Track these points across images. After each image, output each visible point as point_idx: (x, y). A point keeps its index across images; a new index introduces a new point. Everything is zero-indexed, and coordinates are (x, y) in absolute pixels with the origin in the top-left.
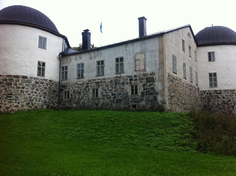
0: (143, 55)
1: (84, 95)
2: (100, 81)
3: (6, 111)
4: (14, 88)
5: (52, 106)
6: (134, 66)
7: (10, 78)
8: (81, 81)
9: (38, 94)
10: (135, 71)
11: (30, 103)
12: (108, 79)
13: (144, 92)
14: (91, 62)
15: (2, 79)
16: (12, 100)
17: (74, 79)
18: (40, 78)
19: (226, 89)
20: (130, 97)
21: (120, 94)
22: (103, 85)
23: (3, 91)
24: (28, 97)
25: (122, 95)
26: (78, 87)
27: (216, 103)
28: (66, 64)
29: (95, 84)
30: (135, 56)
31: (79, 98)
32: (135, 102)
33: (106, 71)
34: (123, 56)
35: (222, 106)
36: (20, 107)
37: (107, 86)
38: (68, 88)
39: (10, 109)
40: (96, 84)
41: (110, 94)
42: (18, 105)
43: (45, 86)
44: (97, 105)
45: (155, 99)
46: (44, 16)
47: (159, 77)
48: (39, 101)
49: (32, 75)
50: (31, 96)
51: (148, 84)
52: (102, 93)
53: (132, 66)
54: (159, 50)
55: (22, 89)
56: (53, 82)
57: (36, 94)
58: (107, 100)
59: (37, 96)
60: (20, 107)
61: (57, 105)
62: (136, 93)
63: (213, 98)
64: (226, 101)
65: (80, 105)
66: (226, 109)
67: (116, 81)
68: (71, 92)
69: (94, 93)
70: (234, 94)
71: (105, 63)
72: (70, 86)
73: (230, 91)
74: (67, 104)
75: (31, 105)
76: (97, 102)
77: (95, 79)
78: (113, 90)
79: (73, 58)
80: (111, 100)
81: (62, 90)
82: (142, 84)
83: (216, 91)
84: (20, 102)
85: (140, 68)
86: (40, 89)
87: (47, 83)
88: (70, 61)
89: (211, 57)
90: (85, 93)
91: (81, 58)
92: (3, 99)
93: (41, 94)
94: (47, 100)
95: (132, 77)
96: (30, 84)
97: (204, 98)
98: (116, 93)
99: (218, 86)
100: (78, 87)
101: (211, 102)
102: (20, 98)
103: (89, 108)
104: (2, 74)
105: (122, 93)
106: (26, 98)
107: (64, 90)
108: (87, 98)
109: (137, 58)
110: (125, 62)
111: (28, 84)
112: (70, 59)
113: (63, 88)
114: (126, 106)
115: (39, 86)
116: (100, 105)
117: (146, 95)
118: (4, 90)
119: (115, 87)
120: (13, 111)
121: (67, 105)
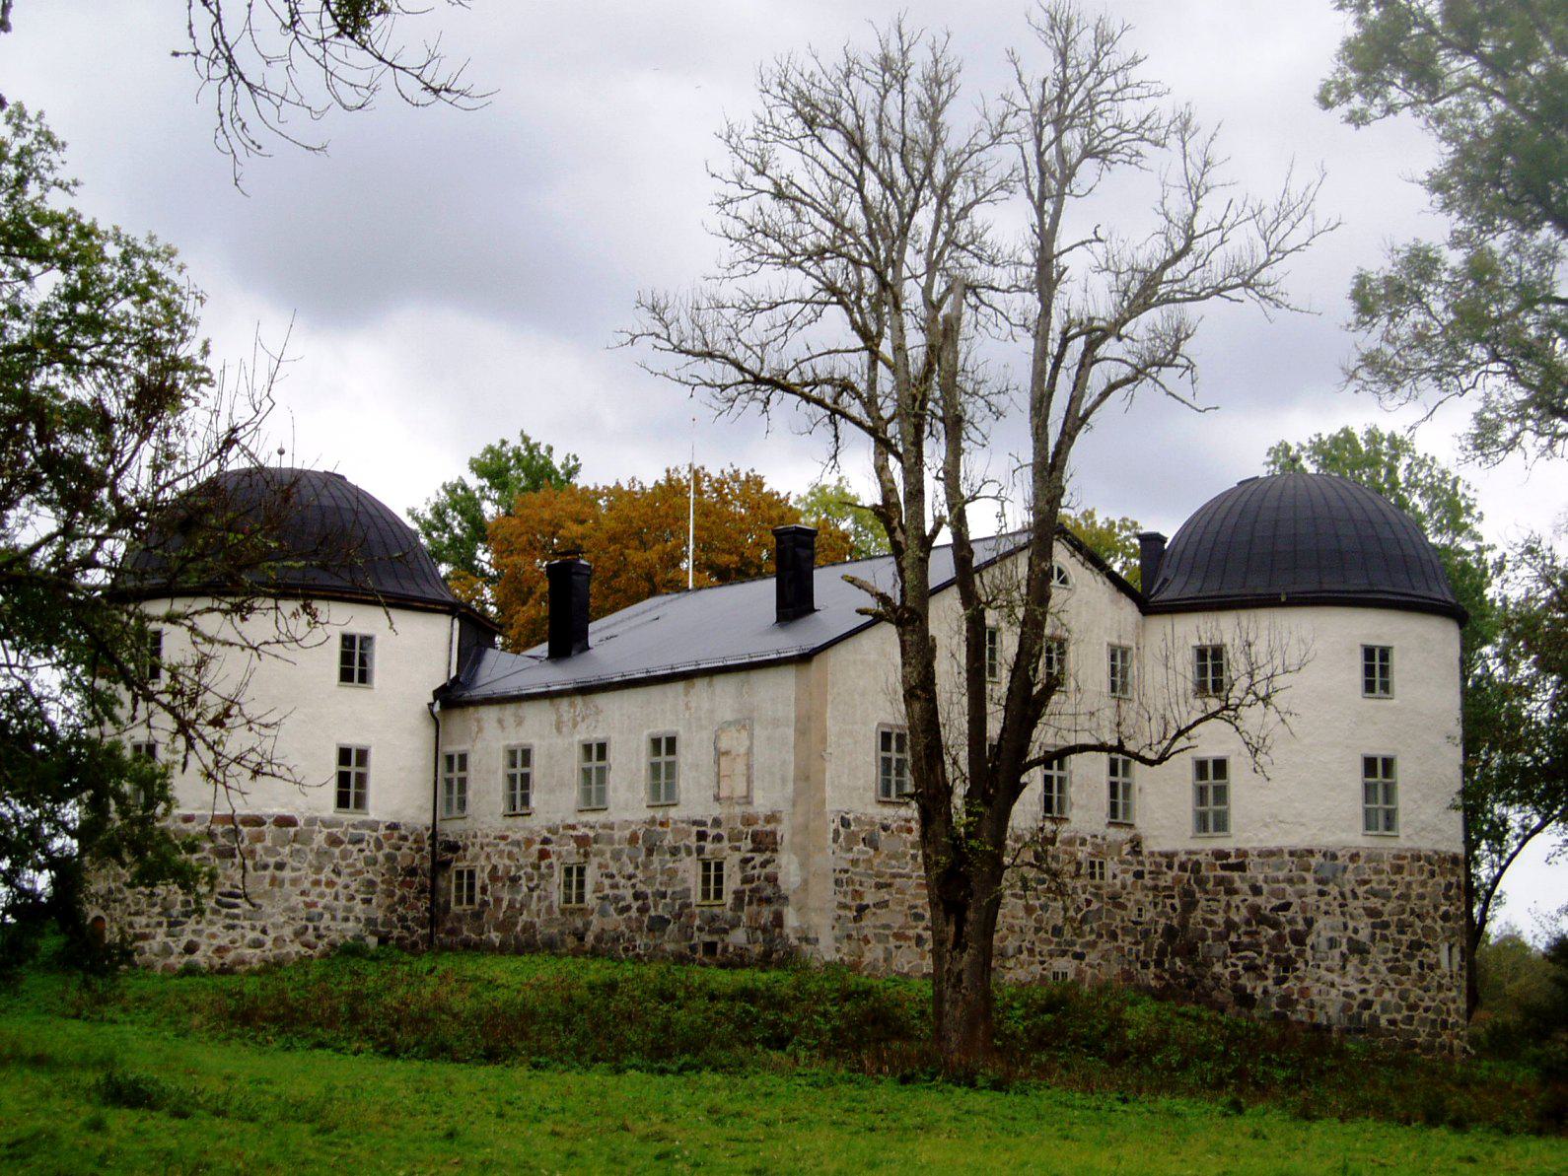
0: (744, 734)
1: (531, 890)
2: (592, 834)
6: (712, 775)
8: (520, 829)
9: (339, 888)
10: (717, 798)
11: (311, 930)
13: (744, 891)
14: (560, 742)
17: (492, 814)
18: (350, 817)
19: (1272, 844)
21: (664, 895)
22: (601, 853)
24: (301, 905)
25: (668, 900)
27: (1219, 919)
29: (573, 845)
30: (717, 738)
31: (511, 905)
32: (711, 932)
33: (615, 790)
34: (675, 729)
35: (1246, 933)
36: (269, 944)
37: (616, 856)
38: (468, 857)
40: (579, 847)
41: (628, 893)
43: (367, 853)
44: (581, 938)
45: (778, 920)
46: (365, 502)
47: (793, 835)
48: (346, 919)
49: (316, 810)
51: (759, 858)
52: (598, 888)
53: (707, 779)
54: (798, 720)
55: (277, 873)
56: (403, 832)
58: (615, 921)
59: (336, 898)
60: (269, 944)
61: (424, 932)
62: (719, 894)
64: (1269, 907)
65: (516, 938)
66: (1266, 949)
67: (648, 842)
68: (482, 877)
69: (568, 885)
70: (1307, 870)
71: (612, 754)
72: (477, 848)
73: (1292, 854)
74: (465, 928)
76: (579, 923)
77: (571, 821)
78: (640, 875)
79: (489, 714)
80: (630, 918)
81: (447, 864)
82: (737, 856)
83: (1221, 855)
85: (733, 790)
86: (348, 866)
90: (535, 882)
91: (520, 723)
93: (354, 886)
94: (380, 915)
95: (704, 824)
96: (307, 849)
97: (1166, 888)
98: (649, 891)
100: (510, 855)
101: (1198, 915)
103: (551, 946)
104: (197, 813)
105: (669, 892)
106: (293, 909)
107: (453, 864)
109: (724, 745)
110: (684, 757)
111: (298, 851)
112: (478, 721)
113: (450, 856)
115: (345, 856)
116: (590, 938)
117: (750, 903)
119: (646, 867)
120: (243, 962)
121: (466, 933)
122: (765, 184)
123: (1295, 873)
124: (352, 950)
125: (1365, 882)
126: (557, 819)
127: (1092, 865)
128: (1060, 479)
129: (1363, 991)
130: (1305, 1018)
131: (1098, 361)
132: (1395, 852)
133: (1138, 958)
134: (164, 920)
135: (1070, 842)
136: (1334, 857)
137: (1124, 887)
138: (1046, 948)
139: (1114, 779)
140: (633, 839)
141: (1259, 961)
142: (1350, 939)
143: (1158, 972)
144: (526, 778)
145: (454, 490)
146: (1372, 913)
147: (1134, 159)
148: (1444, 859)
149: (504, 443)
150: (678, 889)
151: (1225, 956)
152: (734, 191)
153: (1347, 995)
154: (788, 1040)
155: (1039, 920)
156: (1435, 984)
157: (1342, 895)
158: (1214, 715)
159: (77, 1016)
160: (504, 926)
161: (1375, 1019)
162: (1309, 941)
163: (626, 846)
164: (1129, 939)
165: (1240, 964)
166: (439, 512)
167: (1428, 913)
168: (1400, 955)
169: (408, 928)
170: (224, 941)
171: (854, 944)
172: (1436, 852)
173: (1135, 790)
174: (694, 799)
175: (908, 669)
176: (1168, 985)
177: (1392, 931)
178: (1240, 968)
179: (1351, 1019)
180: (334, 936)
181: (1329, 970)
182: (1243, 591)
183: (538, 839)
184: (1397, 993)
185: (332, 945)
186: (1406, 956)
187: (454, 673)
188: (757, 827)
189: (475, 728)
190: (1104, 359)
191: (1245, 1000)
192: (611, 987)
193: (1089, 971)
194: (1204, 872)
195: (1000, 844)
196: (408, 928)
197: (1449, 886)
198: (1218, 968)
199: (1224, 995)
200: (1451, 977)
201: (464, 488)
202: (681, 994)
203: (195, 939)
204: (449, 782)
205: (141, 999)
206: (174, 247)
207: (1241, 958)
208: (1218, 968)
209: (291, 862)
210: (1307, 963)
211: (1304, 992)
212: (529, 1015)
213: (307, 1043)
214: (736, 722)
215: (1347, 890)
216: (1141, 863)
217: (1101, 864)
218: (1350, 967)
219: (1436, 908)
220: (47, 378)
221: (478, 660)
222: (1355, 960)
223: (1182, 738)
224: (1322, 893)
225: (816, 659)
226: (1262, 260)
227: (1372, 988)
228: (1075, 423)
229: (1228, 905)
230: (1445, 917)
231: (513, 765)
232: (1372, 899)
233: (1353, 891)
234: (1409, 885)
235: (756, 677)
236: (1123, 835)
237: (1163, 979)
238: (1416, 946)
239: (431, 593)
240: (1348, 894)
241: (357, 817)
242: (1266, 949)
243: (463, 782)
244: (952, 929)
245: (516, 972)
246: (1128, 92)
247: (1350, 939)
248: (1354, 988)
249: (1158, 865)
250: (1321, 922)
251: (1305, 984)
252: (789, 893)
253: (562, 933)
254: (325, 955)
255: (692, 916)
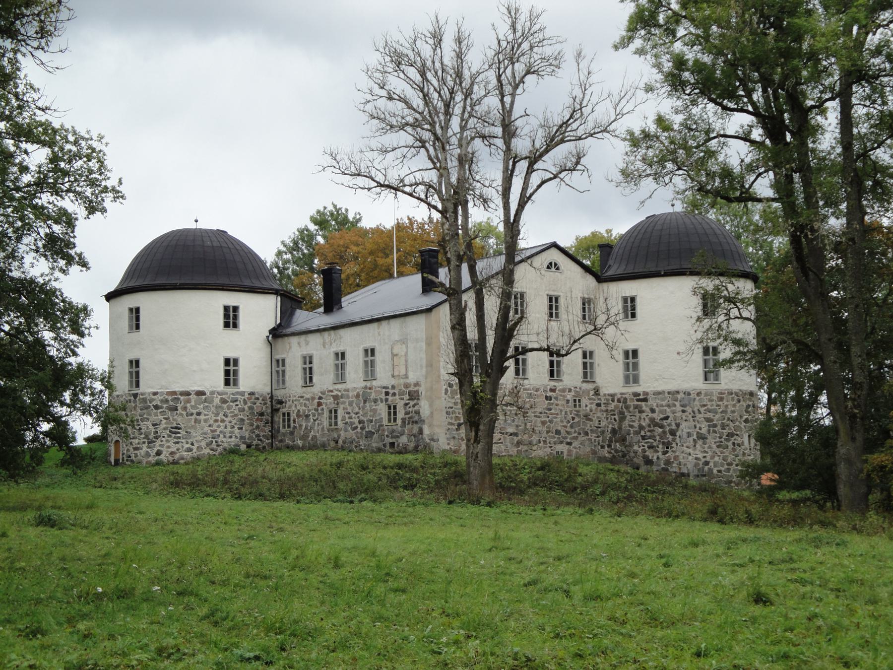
0: (404, 346)
1: (315, 421)
4: (181, 415)
5: (256, 445)
10: (393, 376)
11: (214, 443)
12: (353, 391)
18: (230, 390)
19: (660, 389)
20: (386, 428)
21: (371, 421)
22: (344, 403)
23: (163, 422)
25: (373, 423)
26: (305, 404)
30: (392, 348)
31: (306, 428)
32: (392, 437)
33: (349, 373)
36: (195, 450)
37: (351, 404)
38: (287, 406)
40: (335, 400)
41: (356, 421)
42: (191, 447)
43: (240, 406)
45: (421, 431)
48: (231, 437)
50: (214, 428)
51: (412, 403)
52: (343, 419)
55: (198, 417)
57: (224, 424)
58: (351, 434)
60: (195, 450)
62: (395, 420)
63: (630, 412)
66: (658, 438)
67: (364, 397)
68: (293, 416)
69: (330, 418)
70: (676, 400)
71: (347, 356)
72: (291, 402)
73: (669, 393)
75: (215, 447)
76: (336, 436)
77: (331, 388)
78: (361, 412)
79: (294, 340)
81: (277, 410)
82: (403, 402)
83: (636, 394)
85: (400, 372)
86: (231, 412)
87: (244, 400)
89: (630, 308)
92: (164, 437)
93: (234, 422)
94: (247, 434)
95: (388, 388)
96: (211, 405)
99: (641, 382)
100: (305, 405)
102: (194, 434)
103: (324, 446)
104: (159, 391)
106: (206, 433)
108: (320, 427)
109: (395, 352)
110: (378, 357)
112: (289, 344)
113: (279, 406)
114: (380, 445)
116: (340, 442)
117: (409, 423)
118: (165, 421)
119: (363, 409)
120: (183, 459)
122: (383, 93)
123: (671, 402)
124: (234, 451)
125: (705, 406)
126: (325, 388)
127: (575, 401)
128: (518, 226)
129: (705, 457)
130: (677, 470)
131: (535, 171)
132: (719, 391)
133: (599, 444)
134: (146, 440)
135: (563, 390)
136: (689, 394)
137: (591, 411)
138: (552, 440)
139: (585, 360)
140: (358, 396)
141: (655, 444)
142: (698, 433)
143: (609, 450)
144: (311, 369)
145: (303, 231)
146: (708, 420)
147: (553, 74)
148: (745, 394)
149: (325, 208)
150: (378, 418)
151: (639, 442)
152: (369, 97)
153: (696, 459)
154: (415, 486)
155: (548, 427)
156: (741, 453)
157: (694, 412)
158: (590, 333)
159: (100, 487)
160: (304, 437)
161: (711, 470)
162: (678, 434)
163: (354, 399)
164: (594, 435)
165: (646, 445)
166: (295, 243)
167: (737, 419)
168: (723, 440)
169: (261, 440)
170: (174, 449)
171: (456, 441)
172: (740, 390)
173: (596, 366)
174: (383, 377)
175: (453, 316)
176: (614, 456)
177: (718, 428)
178: (646, 448)
179: (699, 470)
180: (225, 445)
181: (687, 447)
182: (645, 270)
183: (317, 397)
184: (721, 458)
185: (225, 449)
186: (726, 440)
187: (278, 322)
188: (411, 389)
189: (288, 347)
190: (538, 170)
191: (648, 462)
192: (339, 465)
193: (575, 450)
194: (628, 403)
195: (494, 394)
196: (261, 440)
197: (748, 406)
198: (636, 448)
199: (639, 460)
200: (750, 449)
201: (307, 230)
202: (371, 466)
204: (278, 372)
205: (132, 478)
206: (102, 134)
207: (646, 443)
208: (636, 448)
209: (204, 412)
210: (677, 444)
211: (676, 458)
212: (302, 478)
213: (201, 495)
214: (400, 340)
215: (696, 409)
216: (600, 399)
217: (579, 401)
218: (697, 446)
219: (741, 417)
220: (45, 199)
221: (292, 314)
222: (700, 442)
223: (576, 344)
224: (683, 411)
225: (434, 311)
226: (612, 119)
227: (708, 455)
228: (524, 201)
229: (640, 418)
230: (746, 421)
231: (305, 363)
232: (709, 414)
233: (698, 410)
234: (727, 406)
235: (409, 319)
236: (590, 386)
237: (611, 453)
238: (730, 435)
239: (266, 285)
240: (696, 411)
241: (235, 390)
242: (658, 438)
243: (284, 371)
244: (473, 434)
245: (302, 459)
246: (545, 42)
247: (698, 433)
248: (700, 456)
249: (608, 400)
250: (683, 425)
251: (677, 454)
252: (425, 419)
253: (328, 440)
254: (221, 454)
255: (384, 430)
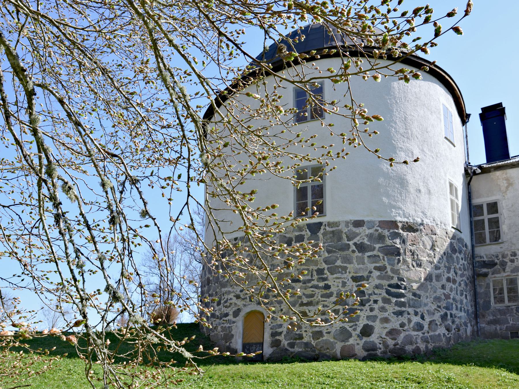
3: (391, 343)
7: (391, 231)
15: (367, 236)
16: (405, 306)
28: (488, 197)
36: (426, 327)
38: (508, 269)
39: (402, 335)
60: (426, 327)
84: (426, 312)
88: (507, 188)
92: (376, 302)
104: (366, 219)
203: (370, 323)
